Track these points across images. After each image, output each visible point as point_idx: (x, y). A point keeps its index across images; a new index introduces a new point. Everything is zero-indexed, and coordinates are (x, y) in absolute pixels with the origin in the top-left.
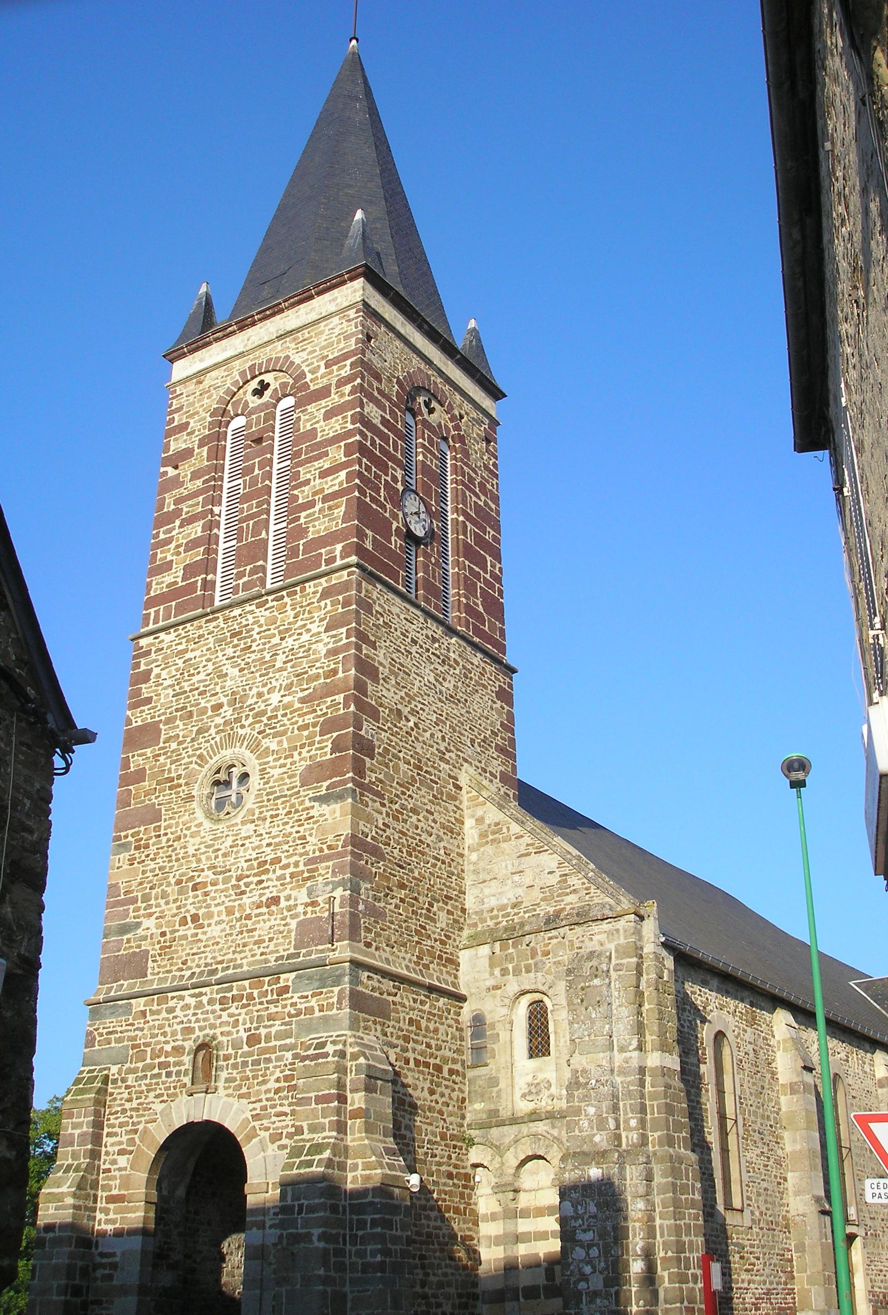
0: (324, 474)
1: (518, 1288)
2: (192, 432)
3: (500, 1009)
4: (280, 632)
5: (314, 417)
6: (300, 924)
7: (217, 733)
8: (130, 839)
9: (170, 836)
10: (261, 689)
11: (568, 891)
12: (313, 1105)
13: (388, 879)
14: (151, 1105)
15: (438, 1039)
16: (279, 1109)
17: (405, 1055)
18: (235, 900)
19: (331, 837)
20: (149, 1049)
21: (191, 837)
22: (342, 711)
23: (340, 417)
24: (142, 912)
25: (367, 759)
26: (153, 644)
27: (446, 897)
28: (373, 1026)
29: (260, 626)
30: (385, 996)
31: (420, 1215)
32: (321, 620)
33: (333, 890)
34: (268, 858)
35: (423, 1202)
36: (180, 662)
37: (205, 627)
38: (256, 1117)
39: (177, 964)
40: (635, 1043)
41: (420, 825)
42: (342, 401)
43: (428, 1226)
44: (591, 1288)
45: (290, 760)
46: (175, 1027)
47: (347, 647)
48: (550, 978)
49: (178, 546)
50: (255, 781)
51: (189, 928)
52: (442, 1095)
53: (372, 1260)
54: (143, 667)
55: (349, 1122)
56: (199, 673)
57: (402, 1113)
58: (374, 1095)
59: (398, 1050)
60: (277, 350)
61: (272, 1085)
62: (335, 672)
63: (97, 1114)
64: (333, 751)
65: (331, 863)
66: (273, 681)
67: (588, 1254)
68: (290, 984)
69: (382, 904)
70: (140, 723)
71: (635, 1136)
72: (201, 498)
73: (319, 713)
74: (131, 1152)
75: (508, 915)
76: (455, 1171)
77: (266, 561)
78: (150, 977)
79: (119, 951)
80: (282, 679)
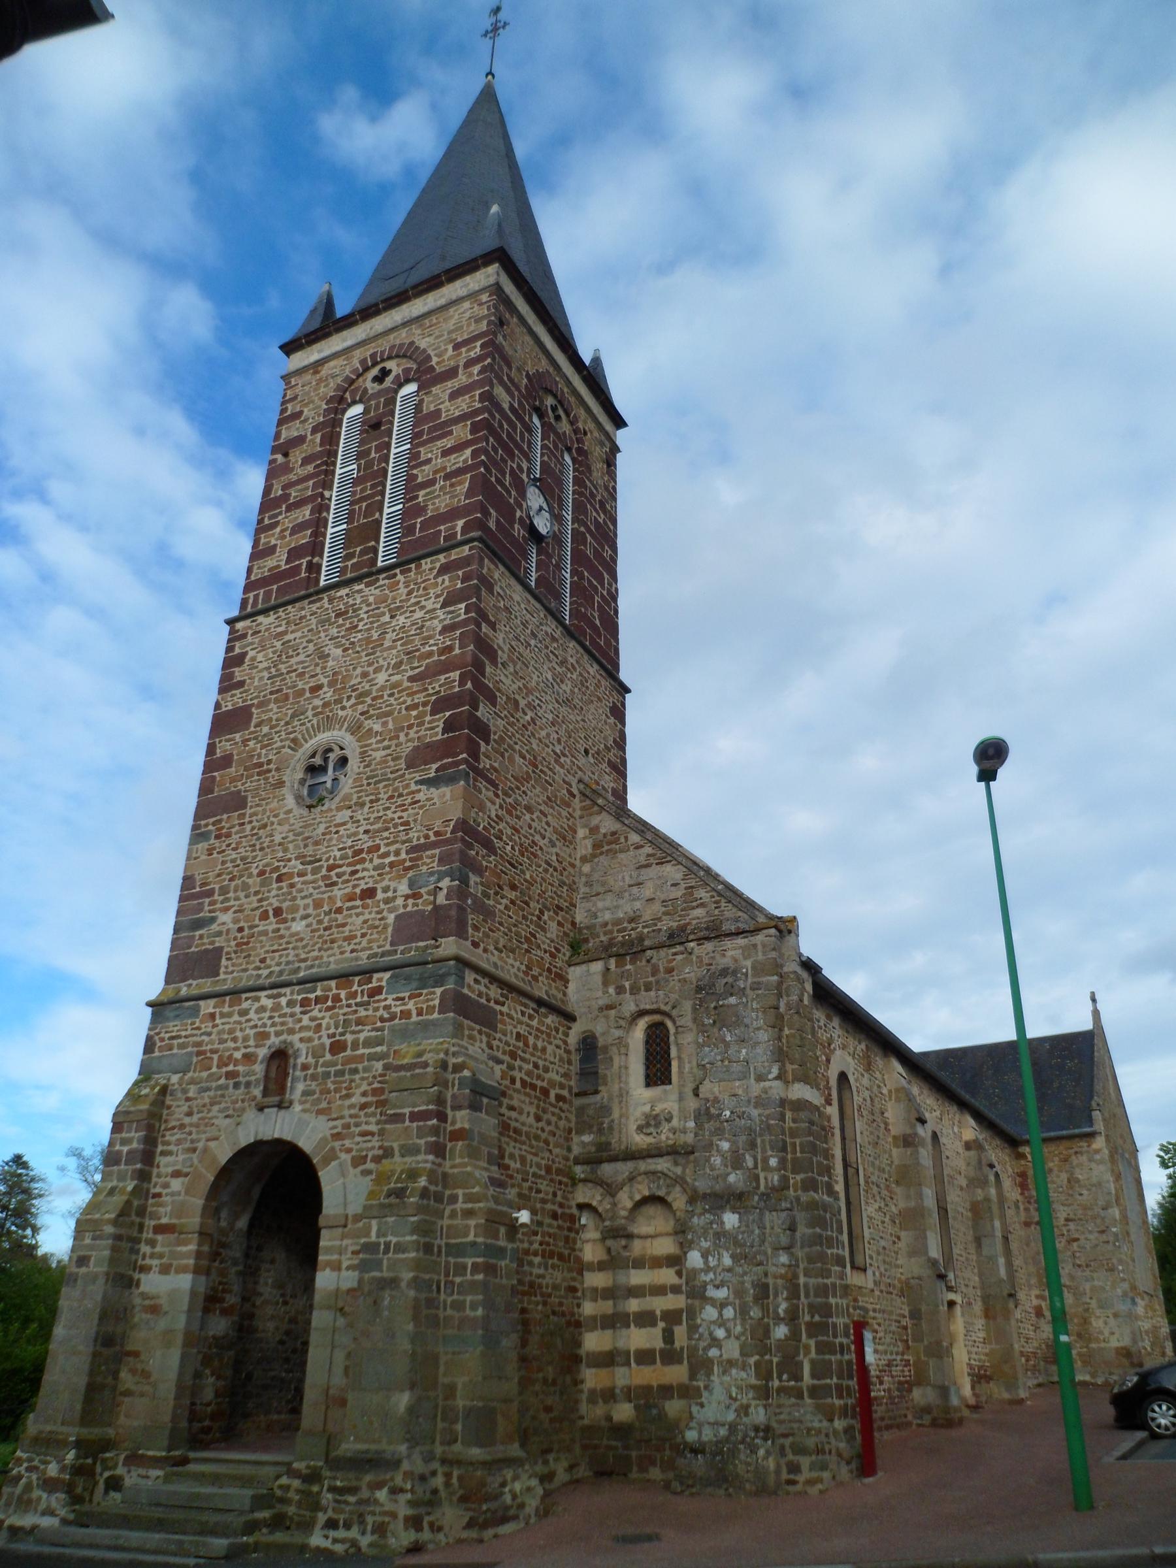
0: (446, 453)
1: (628, 1352)
2: (306, 420)
3: (613, 1030)
4: (390, 610)
5: (440, 399)
6: (397, 917)
7: (314, 715)
8: (210, 827)
9: (255, 823)
10: (366, 669)
11: (694, 904)
12: (407, 1123)
13: (500, 877)
14: (214, 1121)
15: (545, 1060)
16: (364, 1127)
17: (511, 1073)
18: (324, 893)
19: (438, 822)
20: (215, 1057)
21: (279, 824)
22: (457, 689)
23: (467, 397)
24: (218, 906)
25: (482, 743)
26: (250, 628)
27: (558, 907)
28: (478, 1036)
29: (369, 605)
30: (492, 1004)
31: (522, 1260)
32: (437, 596)
33: (439, 880)
34: (365, 846)
35: (526, 1245)
36: (278, 645)
37: (307, 609)
38: (337, 1136)
39: (254, 962)
40: (775, 1071)
41: (534, 824)
42: (471, 381)
43: (531, 1274)
44: (725, 1357)
45: (394, 742)
46: (248, 1031)
47: (465, 623)
48: (674, 996)
49: (282, 531)
50: (354, 765)
51: (271, 923)
52: (549, 1123)
53: (472, 1314)
54: (237, 651)
55: (449, 1145)
56: (298, 654)
57: (507, 1139)
58: (478, 1114)
59: (504, 1067)
60: (402, 337)
61: (357, 1099)
62: (450, 649)
63: (150, 1128)
64: (445, 731)
65: (437, 851)
66: (380, 660)
67: (721, 1315)
68: (384, 983)
69: (491, 903)
70: (230, 708)
71: (776, 1178)
72: (311, 483)
73: (431, 691)
74: (186, 1175)
75: (625, 930)
76: (560, 1211)
77: (378, 542)
78: (222, 976)
79: (190, 947)
80: (392, 657)
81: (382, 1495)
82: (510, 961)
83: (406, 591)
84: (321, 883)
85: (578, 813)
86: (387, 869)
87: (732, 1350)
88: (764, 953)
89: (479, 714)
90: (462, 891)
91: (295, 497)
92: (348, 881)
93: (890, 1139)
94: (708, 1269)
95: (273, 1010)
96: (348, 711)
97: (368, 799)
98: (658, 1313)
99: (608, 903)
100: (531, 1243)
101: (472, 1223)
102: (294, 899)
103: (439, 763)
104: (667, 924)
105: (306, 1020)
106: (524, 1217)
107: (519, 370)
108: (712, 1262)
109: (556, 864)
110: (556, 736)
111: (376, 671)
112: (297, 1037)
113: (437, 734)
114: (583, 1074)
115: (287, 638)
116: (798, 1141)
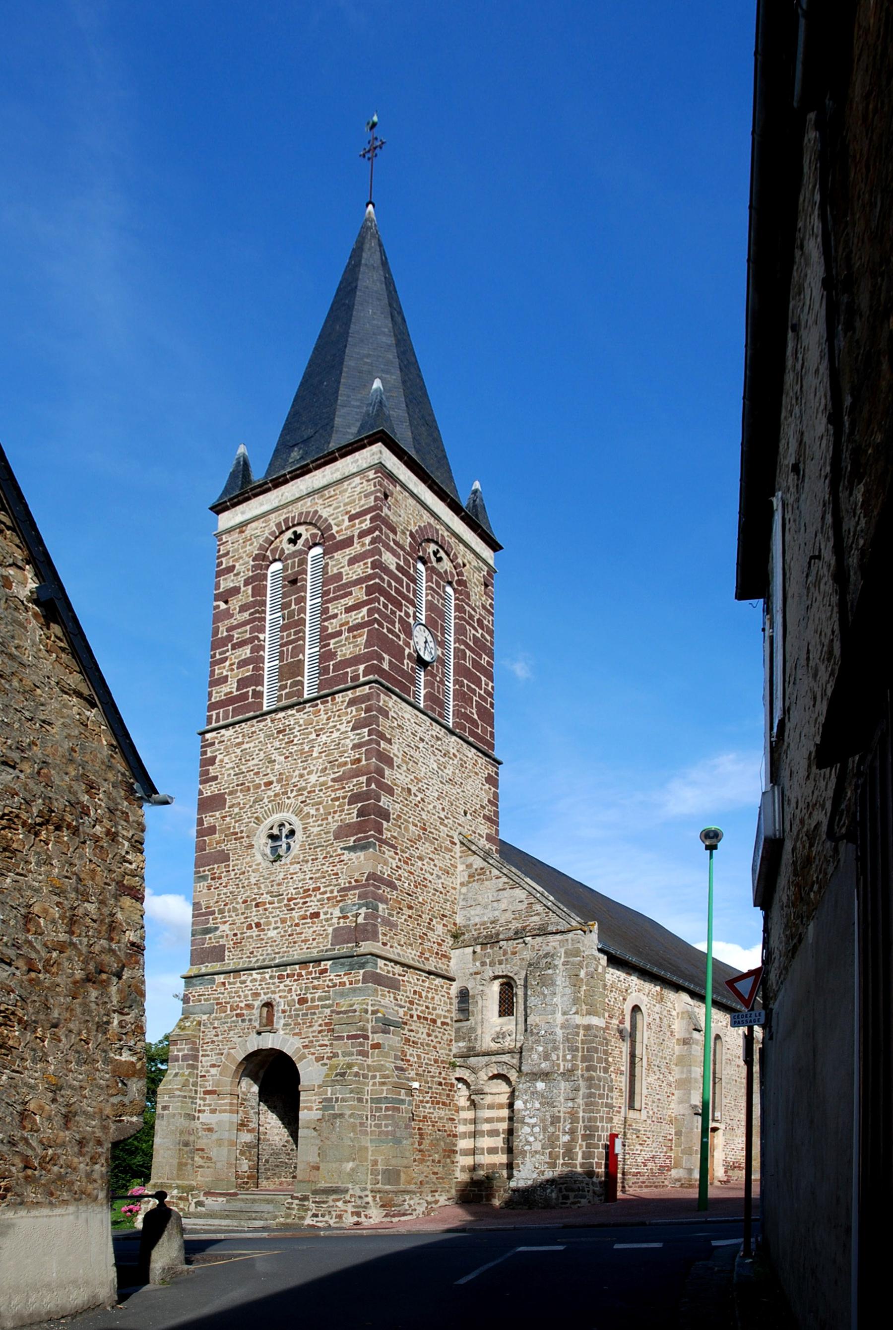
0: (349, 610)
2: (238, 574)
4: (315, 731)
6: (334, 930)
8: (207, 873)
10: (302, 772)
13: (400, 903)
20: (228, 1006)
22: (365, 789)
24: (219, 920)
26: (216, 738)
30: (397, 976)
32: (348, 722)
42: (364, 549)
45: (325, 822)
46: (247, 992)
48: (516, 968)
49: (232, 665)
50: (299, 835)
52: (436, 1037)
54: (209, 755)
59: (406, 1009)
61: (316, 1028)
62: (359, 760)
65: (357, 891)
69: (395, 919)
70: (209, 794)
72: (248, 627)
73: (347, 789)
74: (219, 1066)
76: (443, 1082)
78: (227, 961)
80: (320, 764)
81: (340, 1204)
82: (410, 951)
83: (326, 717)
84: (284, 908)
85: (459, 854)
86: (326, 901)
87: (538, 1146)
88: (572, 944)
89: (381, 804)
90: (373, 915)
91: (238, 638)
92: (301, 908)
93: (675, 1041)
94: (526, 1109)
95: (261, 981)
96: (292, 801)
97: (310, 858)
98: (501, 1131)
99: (477, 912)
100: (424, 1097)
101: (385, 1088)
102: (268, 917)
103: (355, 837)
104: (516, 925)
105: (282, 986)
106: (416, 1085)
107: (404, 533)
108: (529, 1106)
109: (442, 890)
110: (441, 807)
111: (309, 773)
112: (277, 996)
113: (353, 818)
114: (461, 1010)
115: (244, 747)
116: (586, 1046)
